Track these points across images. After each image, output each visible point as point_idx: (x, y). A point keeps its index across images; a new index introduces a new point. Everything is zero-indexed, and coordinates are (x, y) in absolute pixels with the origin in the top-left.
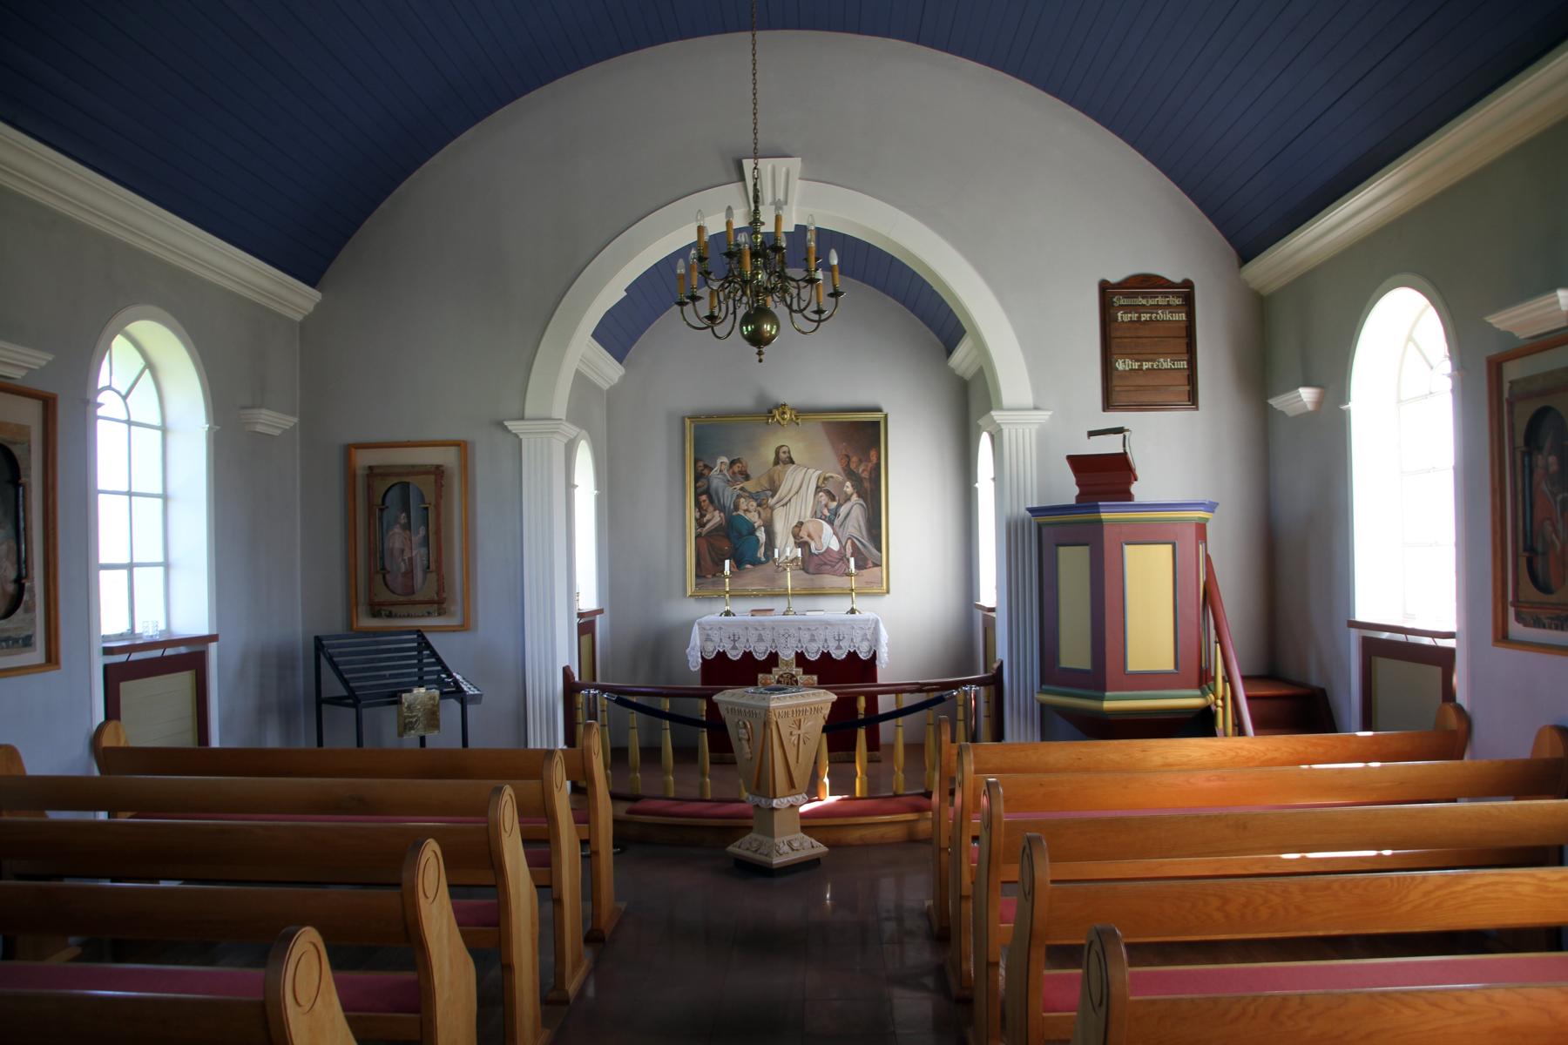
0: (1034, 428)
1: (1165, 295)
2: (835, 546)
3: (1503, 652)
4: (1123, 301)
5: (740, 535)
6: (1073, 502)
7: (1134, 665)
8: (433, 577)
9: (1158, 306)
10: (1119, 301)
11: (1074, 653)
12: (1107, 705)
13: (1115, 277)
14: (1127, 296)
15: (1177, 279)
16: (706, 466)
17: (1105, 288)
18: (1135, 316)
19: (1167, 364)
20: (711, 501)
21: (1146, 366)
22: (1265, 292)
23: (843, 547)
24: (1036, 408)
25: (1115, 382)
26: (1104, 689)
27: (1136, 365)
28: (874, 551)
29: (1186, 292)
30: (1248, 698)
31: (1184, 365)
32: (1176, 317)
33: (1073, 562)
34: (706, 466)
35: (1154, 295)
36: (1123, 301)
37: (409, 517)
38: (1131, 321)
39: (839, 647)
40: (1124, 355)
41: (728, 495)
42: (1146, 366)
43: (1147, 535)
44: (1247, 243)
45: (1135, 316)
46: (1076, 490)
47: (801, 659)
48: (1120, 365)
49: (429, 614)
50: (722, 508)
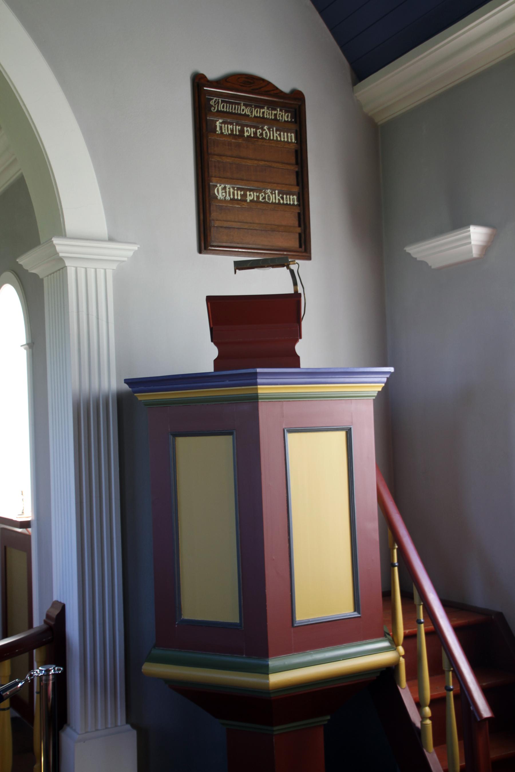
0: (111, 268)
1: (272, 106)
3: (346, 425)
6: (209, 368)
7: (306, 611)
9: (263, 120)
10: (217, 105)
11: (208, 592)
12: (275, 679)
14: (227, 99)
15: (285, 87)
17: (199, 82)
19: (274, 198)
21: (251, 196)
22: (380, 120)
24: (111, 239)
25: (214, 215)
26: (265, 654)
27: (238, 195)
29: (294, 104)
31: (293, 200)
33: (202, 466)
35: (259, 104)
42: (251, 196)
44: (363, 58)
46: (214, 352)
48: (222, 192)
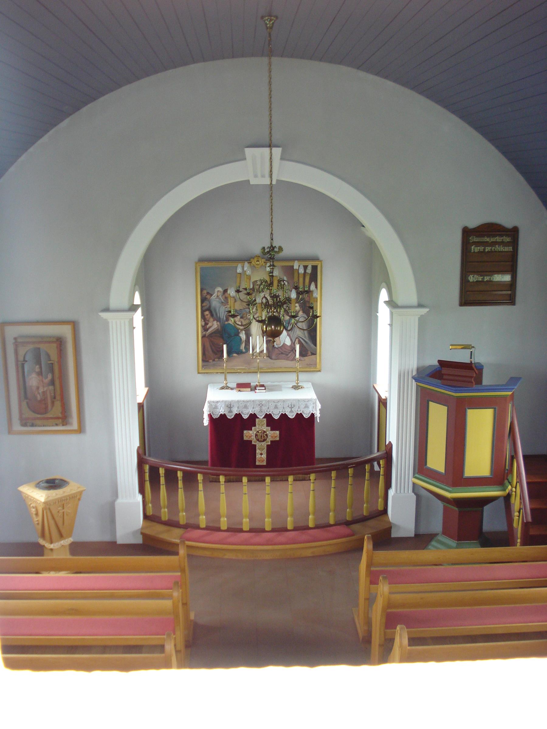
1: (501, 236)
2: (288, 342)
4: (476, 239)
5: (230, 336)
8: (58, 404)
13: (473, 224)
16: (208, 293)
17: (467, 232)
18: (482, 248)
20: (212, 315)
23: (293, 344)
27: (480, 279)
28: (312, 345)
30: (528, 483)
32: (506, 249)
34: (208, 293)
36: (476, 239)
37: (41, 367)
38: (479, 252)
39: (291, 411)
40: (474, 272)
41: (222, 312)
43: (480, 403)
45: (482, 248)
47: (268, 417)
49: (57, 425)
50: (218, 320)
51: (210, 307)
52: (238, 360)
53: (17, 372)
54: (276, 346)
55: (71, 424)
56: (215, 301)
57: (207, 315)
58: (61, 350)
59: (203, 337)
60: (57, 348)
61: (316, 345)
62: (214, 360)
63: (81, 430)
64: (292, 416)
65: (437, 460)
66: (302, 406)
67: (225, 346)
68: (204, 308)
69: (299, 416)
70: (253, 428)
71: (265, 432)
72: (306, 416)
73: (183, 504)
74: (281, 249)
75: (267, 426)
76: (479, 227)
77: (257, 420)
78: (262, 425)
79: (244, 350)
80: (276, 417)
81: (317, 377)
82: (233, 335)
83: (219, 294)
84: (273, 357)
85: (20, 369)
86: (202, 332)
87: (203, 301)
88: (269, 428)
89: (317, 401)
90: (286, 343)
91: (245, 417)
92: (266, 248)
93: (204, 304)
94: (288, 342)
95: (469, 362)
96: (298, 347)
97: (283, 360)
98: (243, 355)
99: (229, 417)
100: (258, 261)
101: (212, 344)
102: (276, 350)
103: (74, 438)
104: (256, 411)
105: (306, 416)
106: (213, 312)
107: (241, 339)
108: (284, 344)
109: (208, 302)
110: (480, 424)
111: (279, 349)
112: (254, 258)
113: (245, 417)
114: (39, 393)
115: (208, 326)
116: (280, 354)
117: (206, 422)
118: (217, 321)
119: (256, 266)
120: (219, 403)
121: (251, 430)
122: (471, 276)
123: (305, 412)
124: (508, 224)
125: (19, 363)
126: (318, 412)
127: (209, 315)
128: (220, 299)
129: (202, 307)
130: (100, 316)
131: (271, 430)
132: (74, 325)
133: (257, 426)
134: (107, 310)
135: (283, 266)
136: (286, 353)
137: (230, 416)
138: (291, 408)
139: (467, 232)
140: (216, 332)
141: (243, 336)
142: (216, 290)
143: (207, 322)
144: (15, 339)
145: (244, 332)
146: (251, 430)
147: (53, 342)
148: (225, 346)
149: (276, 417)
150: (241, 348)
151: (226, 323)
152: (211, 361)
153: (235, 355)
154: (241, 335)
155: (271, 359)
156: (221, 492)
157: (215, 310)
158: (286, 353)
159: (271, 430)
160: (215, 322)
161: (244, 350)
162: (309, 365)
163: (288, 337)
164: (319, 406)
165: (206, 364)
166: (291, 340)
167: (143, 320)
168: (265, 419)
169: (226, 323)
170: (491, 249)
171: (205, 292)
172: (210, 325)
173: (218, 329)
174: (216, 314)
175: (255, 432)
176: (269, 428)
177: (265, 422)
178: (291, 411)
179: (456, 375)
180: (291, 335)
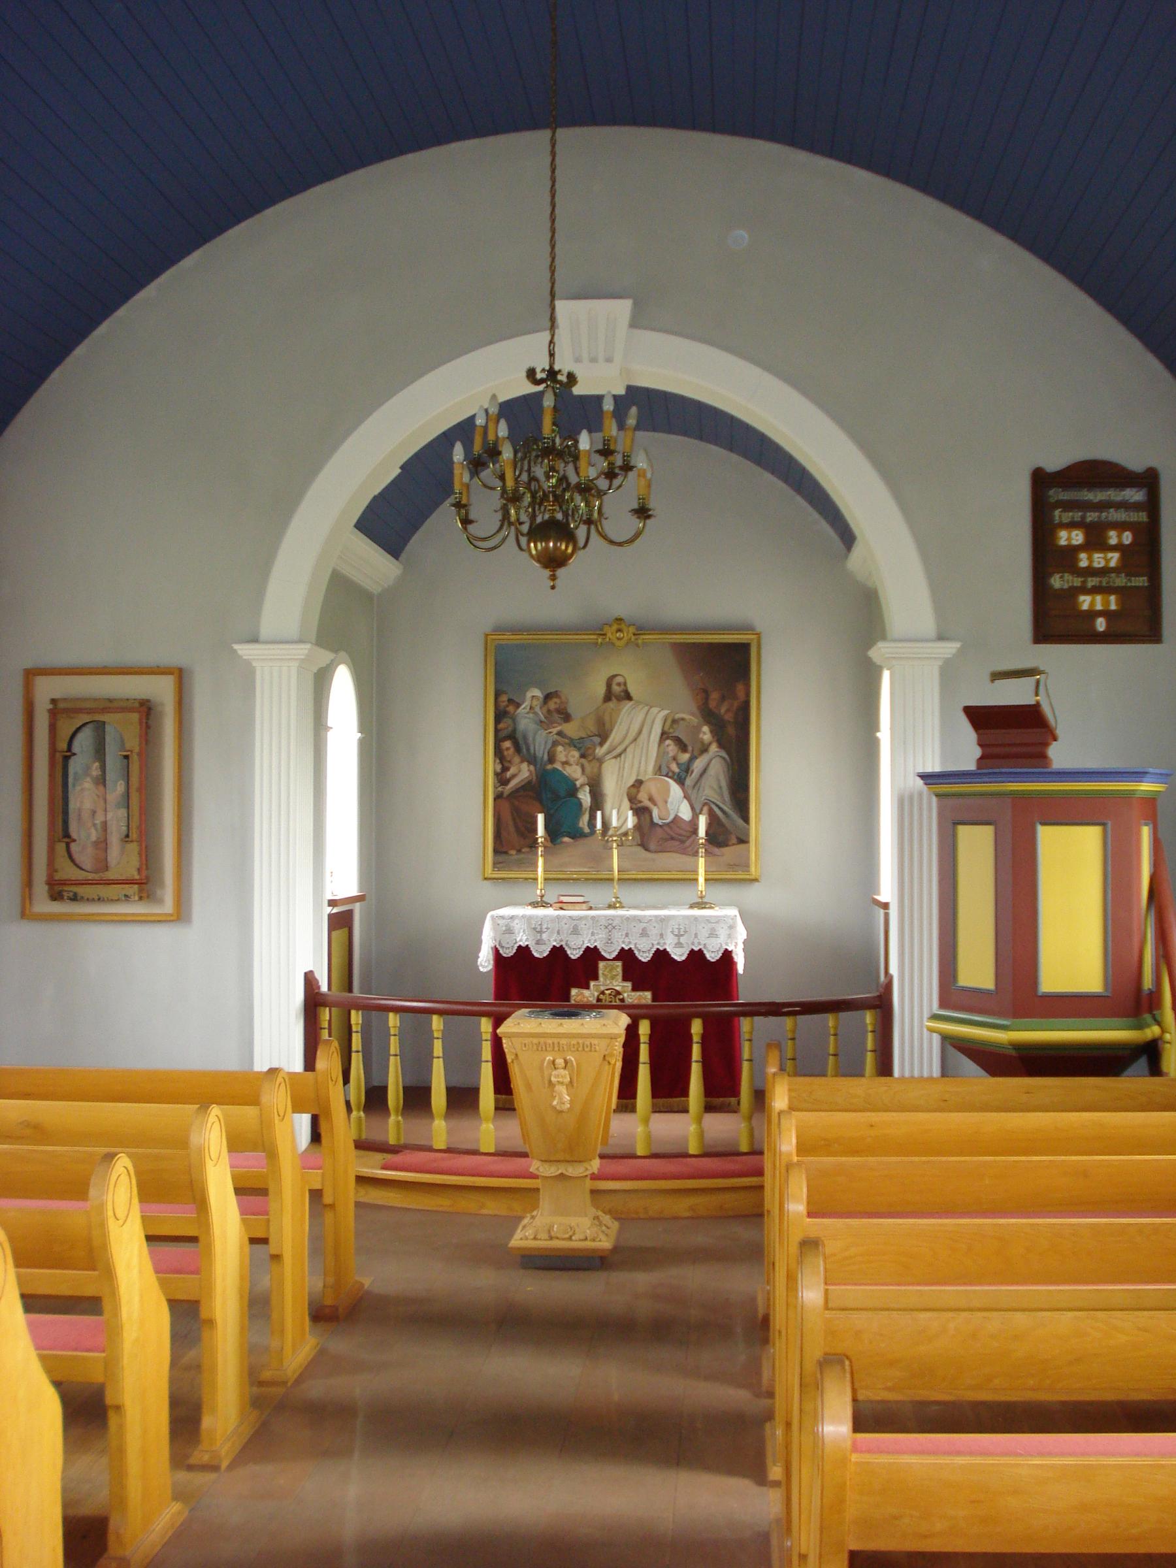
2: (685, 813)
5: (556, 797)
13: (1054, 463)
16: (510, 701)
17: (1041, 480)
20: (518, 749)
28: (740, 822)
34: (510, 701)
41: (540, 741)
43: (1069, 811)
47: (626, 956)
50: (532, 760)
51: (514, 730)
52: (572, 853)
53: (52, 776)
54: (656, 820)
55: (160, 901)
56: (526, 719)
57: (508, 749)
58: (148, 727)
59: (498, 797)
60: (141, 723)
61: (746, 819)
62: (519, 851)
63: (181, 914)
64: (679, 955)
65: (978, 969)
66: (704, 933)
67: (540, 818)
68: (502, 734)
69: (697, 956)
70: (592, 984)
71: (618, 993)
72: (712, 956)
73: (398, 1099)
74: (572, 378)
75: (625, 979)
76: (1069, 468)
77: (601, 964)
78: (613, 978)
79: (587, 830)
80: (645, 957)
81: (753, 895)
82: (562, 793)
83: (535, 703)
84: (652, 846)
85: (59, 768)
86: (495, 787)
87: (500, 715)
88: (629, 985)
89: (738, 918)
90: (680, 815)
91: (574, 954)
92: (538, 370)
93: (501, 726)
94: (685, 813)
95: (1033, 703)
96: (703, 822)
97: (674, 855)
98: (581, 842)
99: (536, 955)
100: (619, 630)
101: (516, 812)
102: (659, 830)
103: (162, 934)
104: (596, 941)
105: (712, 956)
106: (521, 742)
107: (580, 804)
108: (677, 818)
109: (510, 721)
110: (1072, 863)
111: (666, 828)
112: (610, 626)
113: (574, 954)
114: (95, 825)
115: (508, 774)
116: (666, 840)
117: (485, 961)
118: (530, 763)
119: (618, 643)
120: (516, 921)
121: (588, 987)
122: (1057, 576)
123: (710, 948)
124: (1135, 462)
125: (58, 755)
126: (741, 946)
127: (512, 750)
128: (535, 713)
129: (497, 731)
130: (235, 651)
131: (634, 989)
132: (181, 676)
133: (601, 979)
134: (255, 640)
135: (675, 644)
136: (677, 837)
137: (540, 952)
138: (679, 936)
139: (1041, 480)
140: (526, 787)
141: (585, 797)
142: (529, 695)
143: (506, 764)
144: (53, 701)
145: (587, 789)
146: (588, 987)
147: (131, 710)
148: (540, 818)
149: (645, 957)
150: (581, 825)
151: (549, 767)
152: (513, 852)
153: (566, 839)
154: (581, 795)
155: (646, 850)
156: (484, 1059)
157: (525, 738)
158: (677, 837)
159: (634, 989)
160: (525, 766)
161: (587, 830)
162: (733, 866)
163: (685, 801)
164: (741, 933)
165: (501, 858)
166: (693, 808)
167: (362, 744)
168: (619, 964)
169: (549, 767)
170: (1099, 517)
171: (504, 698)
172: (512, 771)
173: (529, 782)
174: (528, 750)
175: (596, 994)
176: (629, 985)
177: (620, 970)
178: (679, 945)
179: (1009, 745)
180: (693, 797)
